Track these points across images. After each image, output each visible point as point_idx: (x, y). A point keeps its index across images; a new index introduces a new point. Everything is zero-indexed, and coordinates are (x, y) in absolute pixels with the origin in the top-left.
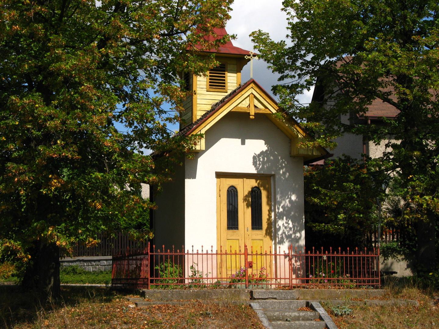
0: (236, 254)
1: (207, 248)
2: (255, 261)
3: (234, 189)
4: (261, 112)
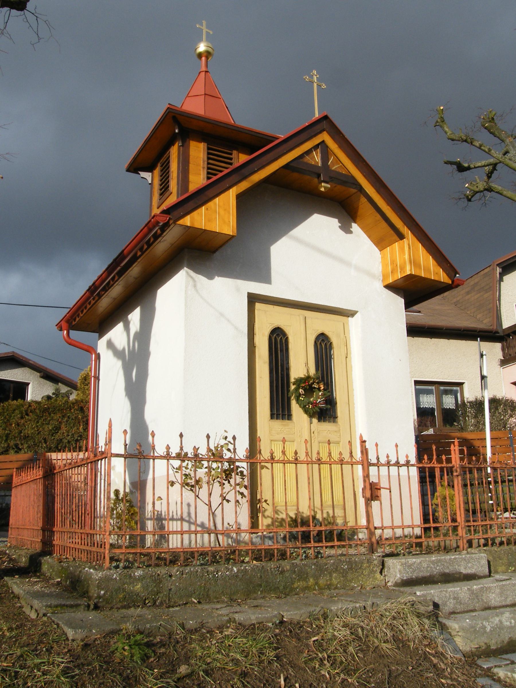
0: (342, 462)
2: (384, 483)
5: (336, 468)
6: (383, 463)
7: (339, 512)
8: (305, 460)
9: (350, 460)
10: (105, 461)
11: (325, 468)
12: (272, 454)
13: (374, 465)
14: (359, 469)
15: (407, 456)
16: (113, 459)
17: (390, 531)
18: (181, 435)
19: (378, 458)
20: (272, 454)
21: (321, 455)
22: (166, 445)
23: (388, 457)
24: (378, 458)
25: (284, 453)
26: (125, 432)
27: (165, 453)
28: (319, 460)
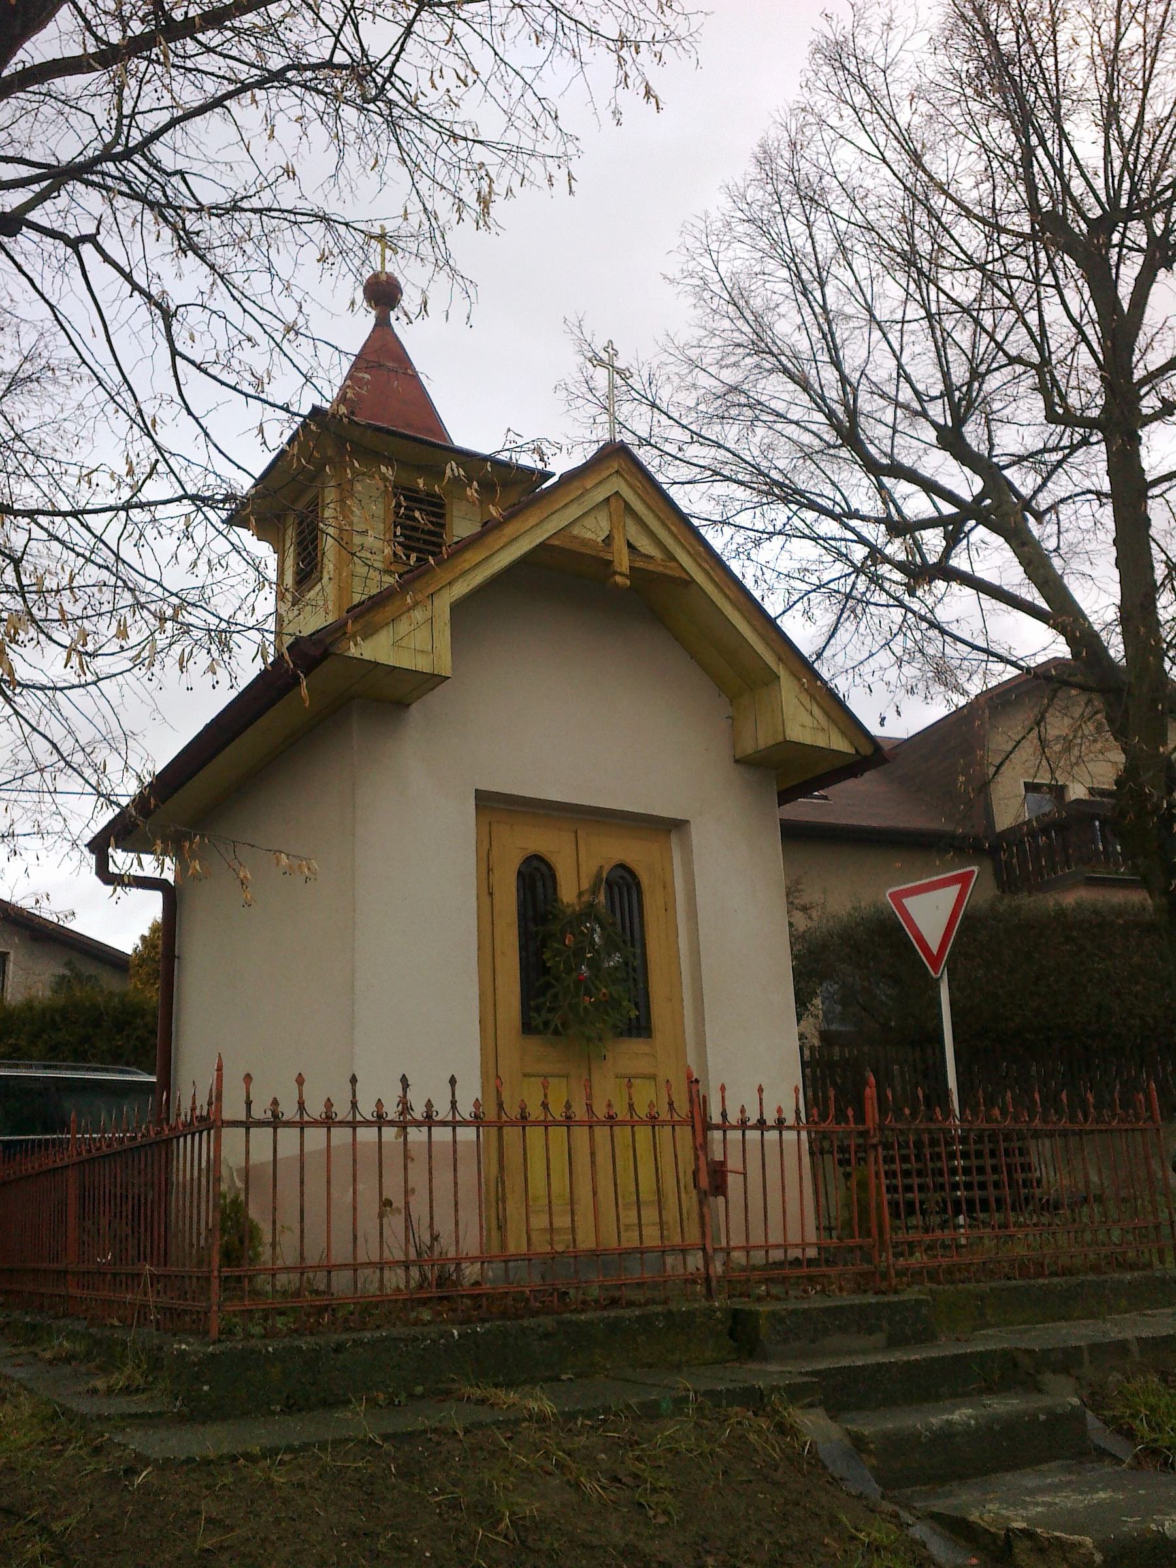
0: (569, 1121)
1: (788, 732)
2: (734, 1163)
3: (543, 867)
4: (651, 567)
5: (602, 1133)
6: (734, 1123)
7: (445, 1227)
8: (542, 1118)
9: (628, 1118)
10: (209, 1135)
11: (581, 1135)
12: (523, 1109)
13: (717, 1127)
14: (683, 1133)
15: (780, 1110)
16: (225, 1131)
17: (295, 1277)
18: (453, 1081)
19: (724, 1115)
20: (523, 1109)
21: (747, 1114)
22: (425, 1101)
23: (743, 1111)
24: (724, 1115)
25: (545, 1105)
26: (796, 1090)
27: (324, 1116)
28: (568, 1118)
